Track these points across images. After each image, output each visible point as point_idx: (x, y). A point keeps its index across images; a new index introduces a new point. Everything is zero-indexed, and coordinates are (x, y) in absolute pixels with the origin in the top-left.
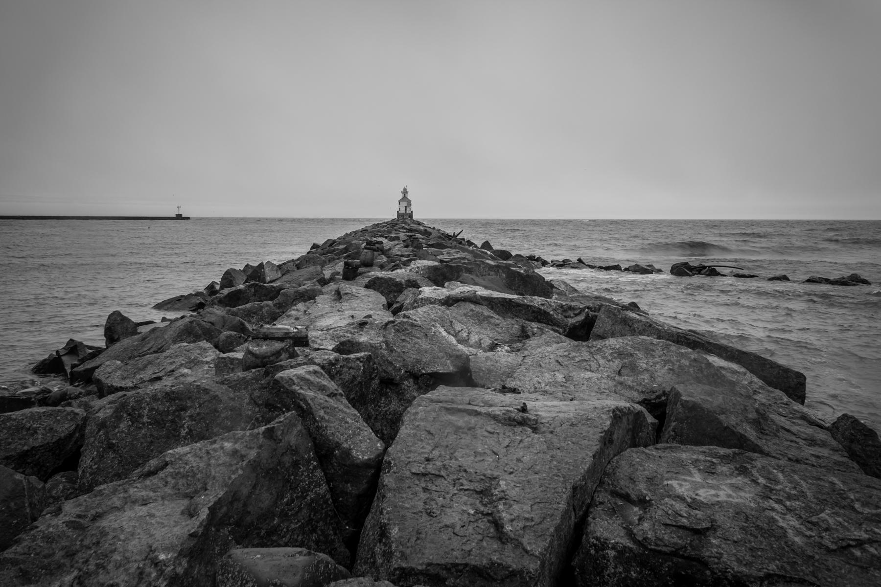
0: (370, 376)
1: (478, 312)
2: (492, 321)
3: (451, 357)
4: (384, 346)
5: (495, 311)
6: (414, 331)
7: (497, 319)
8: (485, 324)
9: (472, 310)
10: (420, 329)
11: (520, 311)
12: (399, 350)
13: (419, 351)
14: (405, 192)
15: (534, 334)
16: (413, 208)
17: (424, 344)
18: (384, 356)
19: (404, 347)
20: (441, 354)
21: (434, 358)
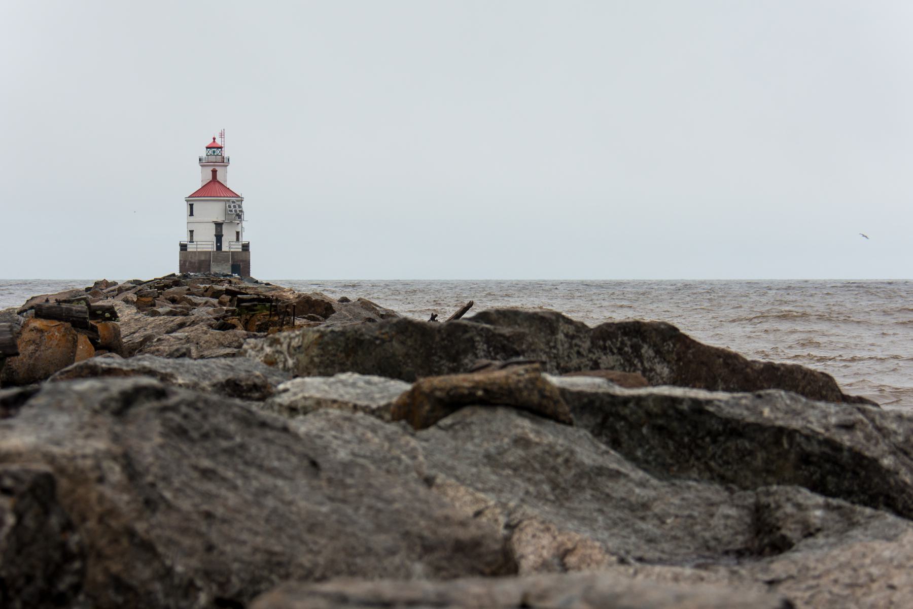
0: (52, 578)
1: (551, 451)
2: (618, 489)
3: (428, 548)
4: (115, 473)
5: (630, 456)
6: (256, 446)
7: (636, 482)
8: (585, 502)
9: (522, 442)
10: (284, 439)
11: (743, 455)
12: (185, 505)
13: (279, 523)
14: (215, 157)
15: (809, 532)
16: (251, 231)
17: (303, 497)
18: (112, 512)
19: (208, 496)
20: (382, 541)
21: (351, 552)
